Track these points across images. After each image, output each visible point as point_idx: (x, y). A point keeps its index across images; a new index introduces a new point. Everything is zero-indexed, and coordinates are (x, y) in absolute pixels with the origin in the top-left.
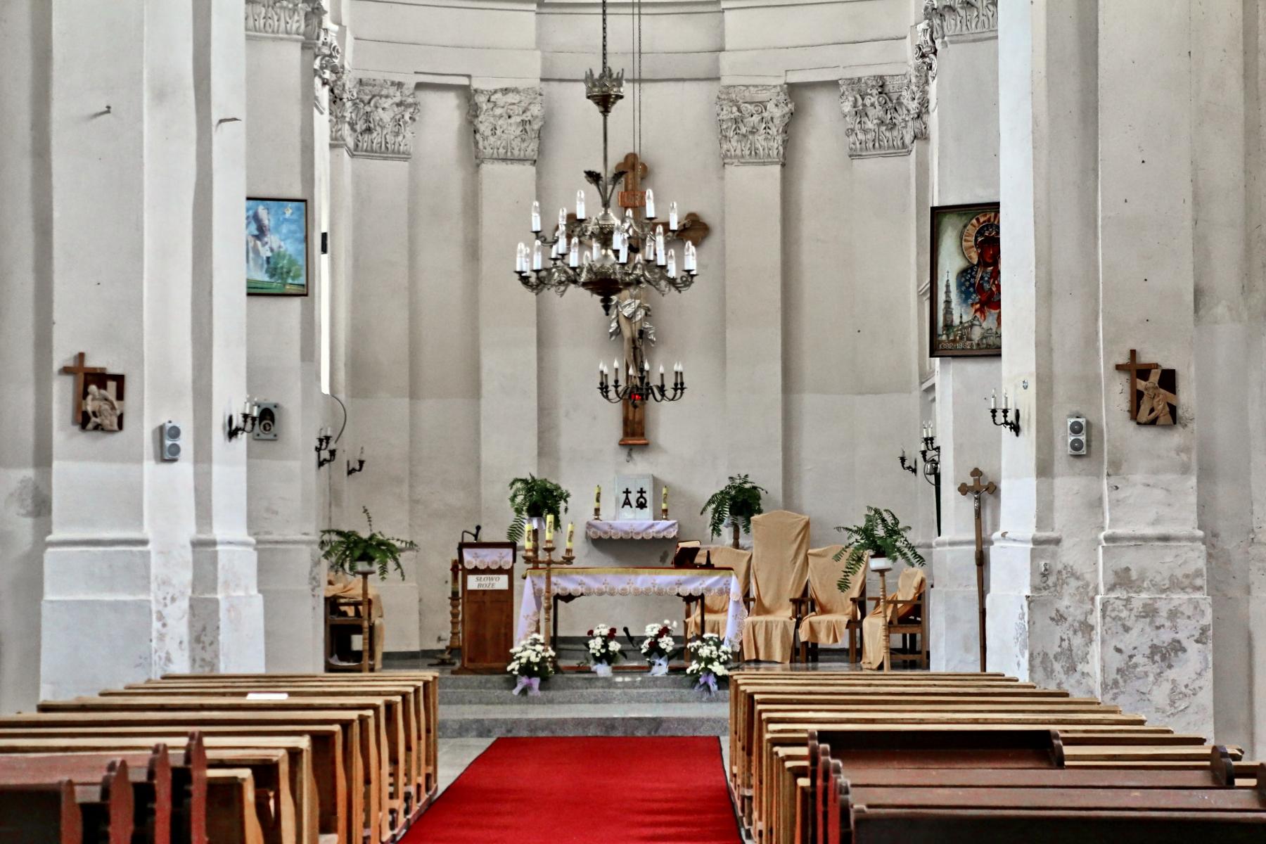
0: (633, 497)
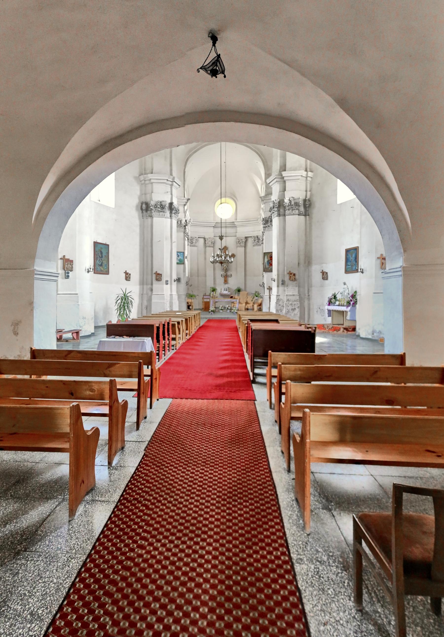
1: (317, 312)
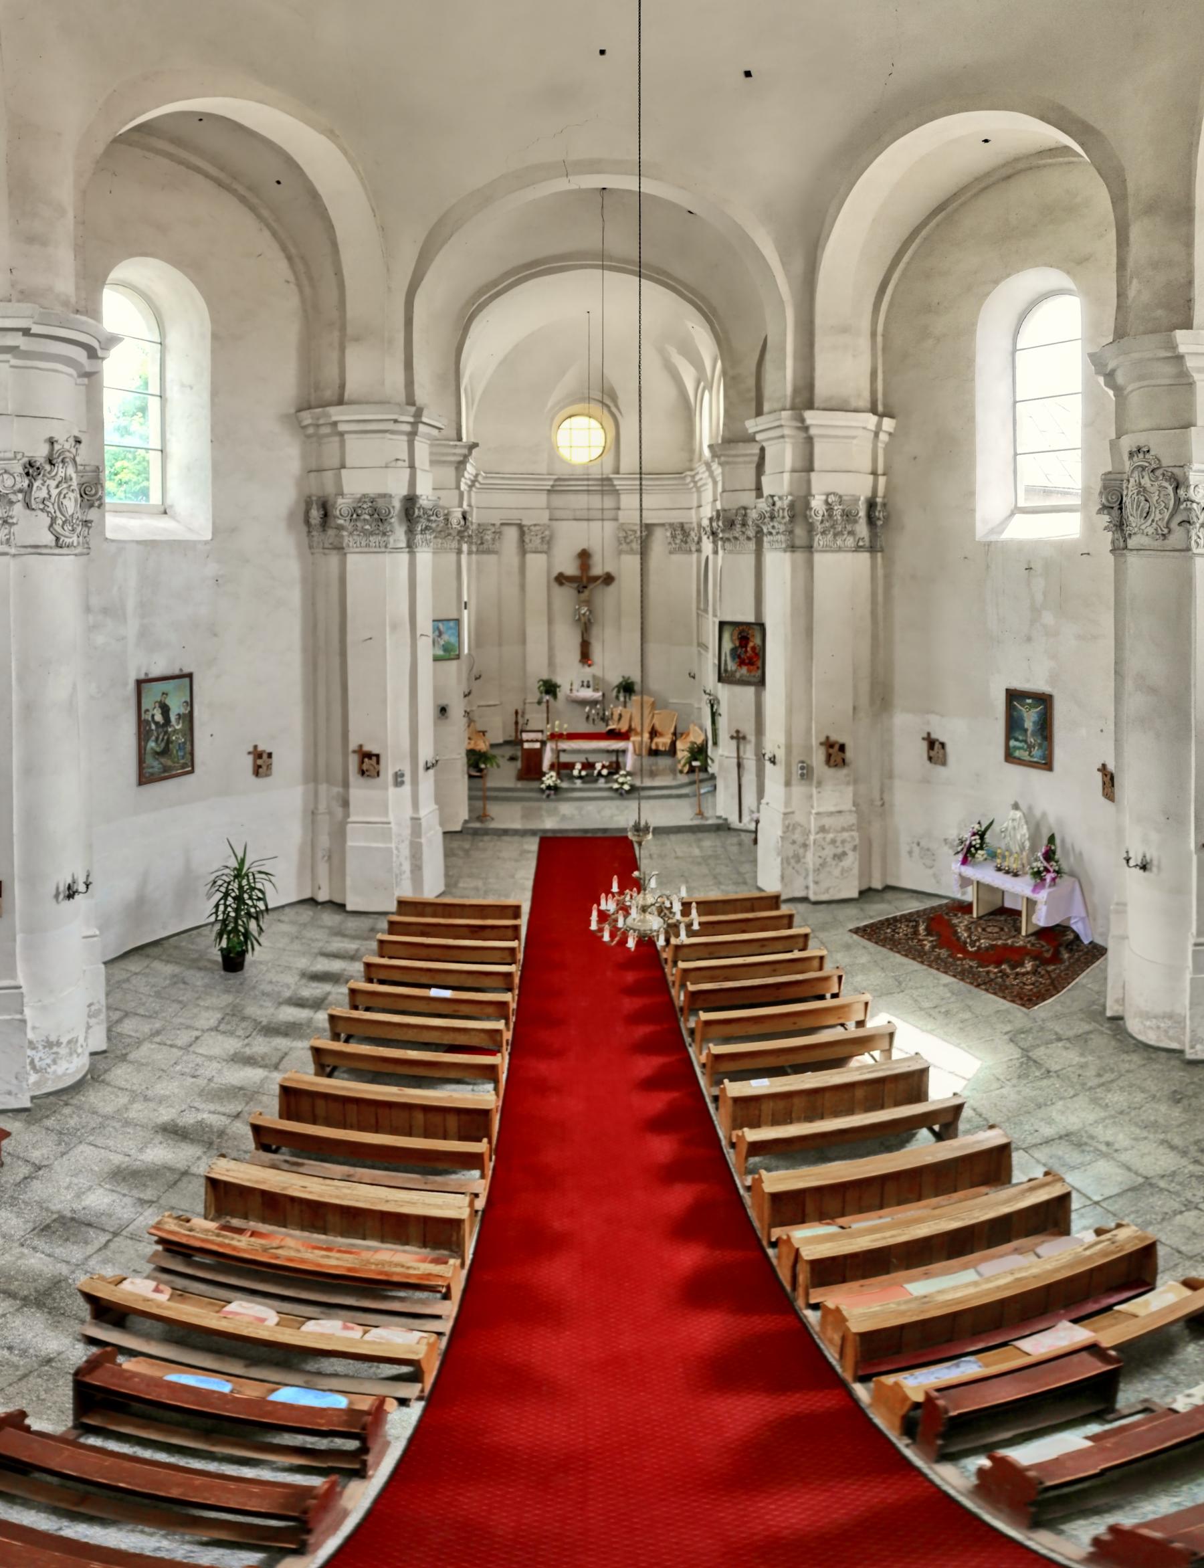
0: (585, 684)
1: (910, 853)
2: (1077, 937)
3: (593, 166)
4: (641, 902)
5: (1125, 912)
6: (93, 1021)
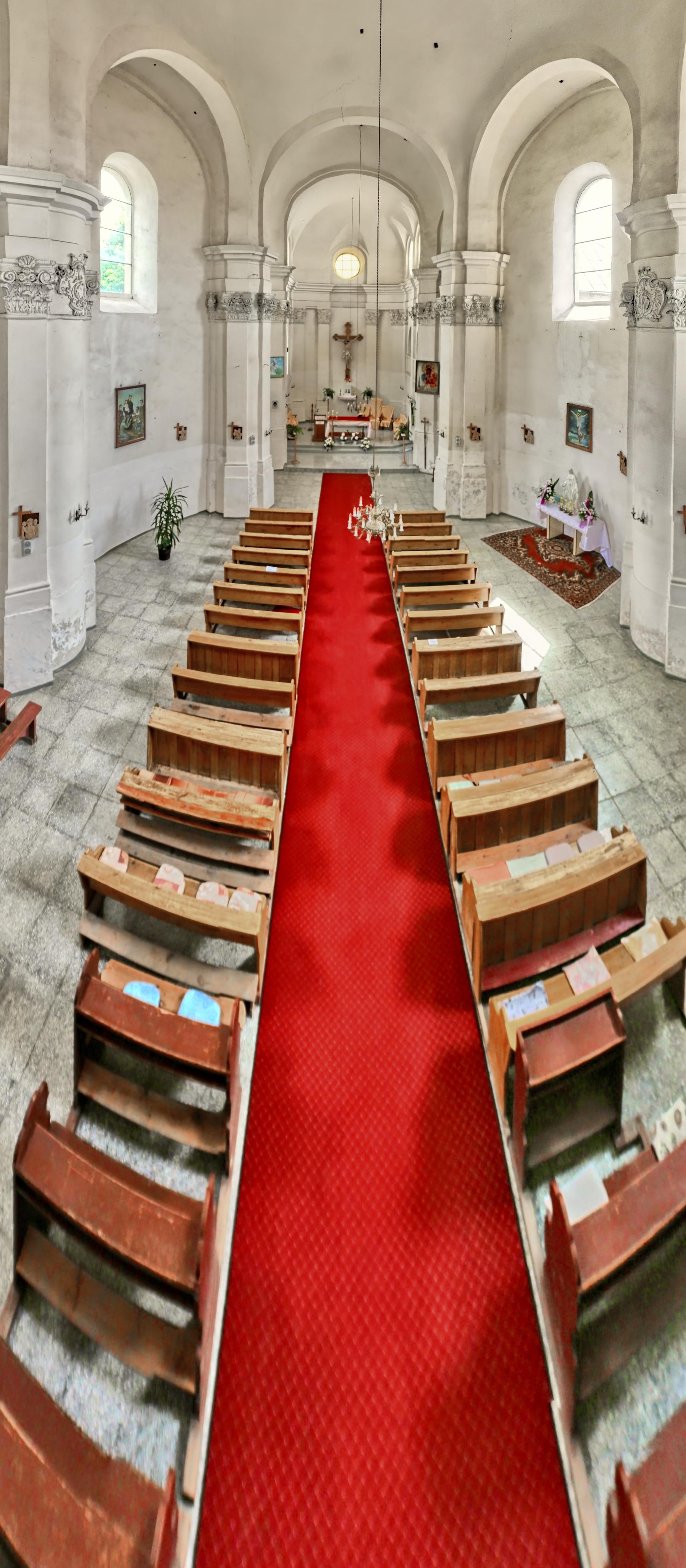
1: (514, 494)
2: (604, 561)
3: (356, 111)
4: (374, 513)
5: (631, 549)
6: (88, 604)
